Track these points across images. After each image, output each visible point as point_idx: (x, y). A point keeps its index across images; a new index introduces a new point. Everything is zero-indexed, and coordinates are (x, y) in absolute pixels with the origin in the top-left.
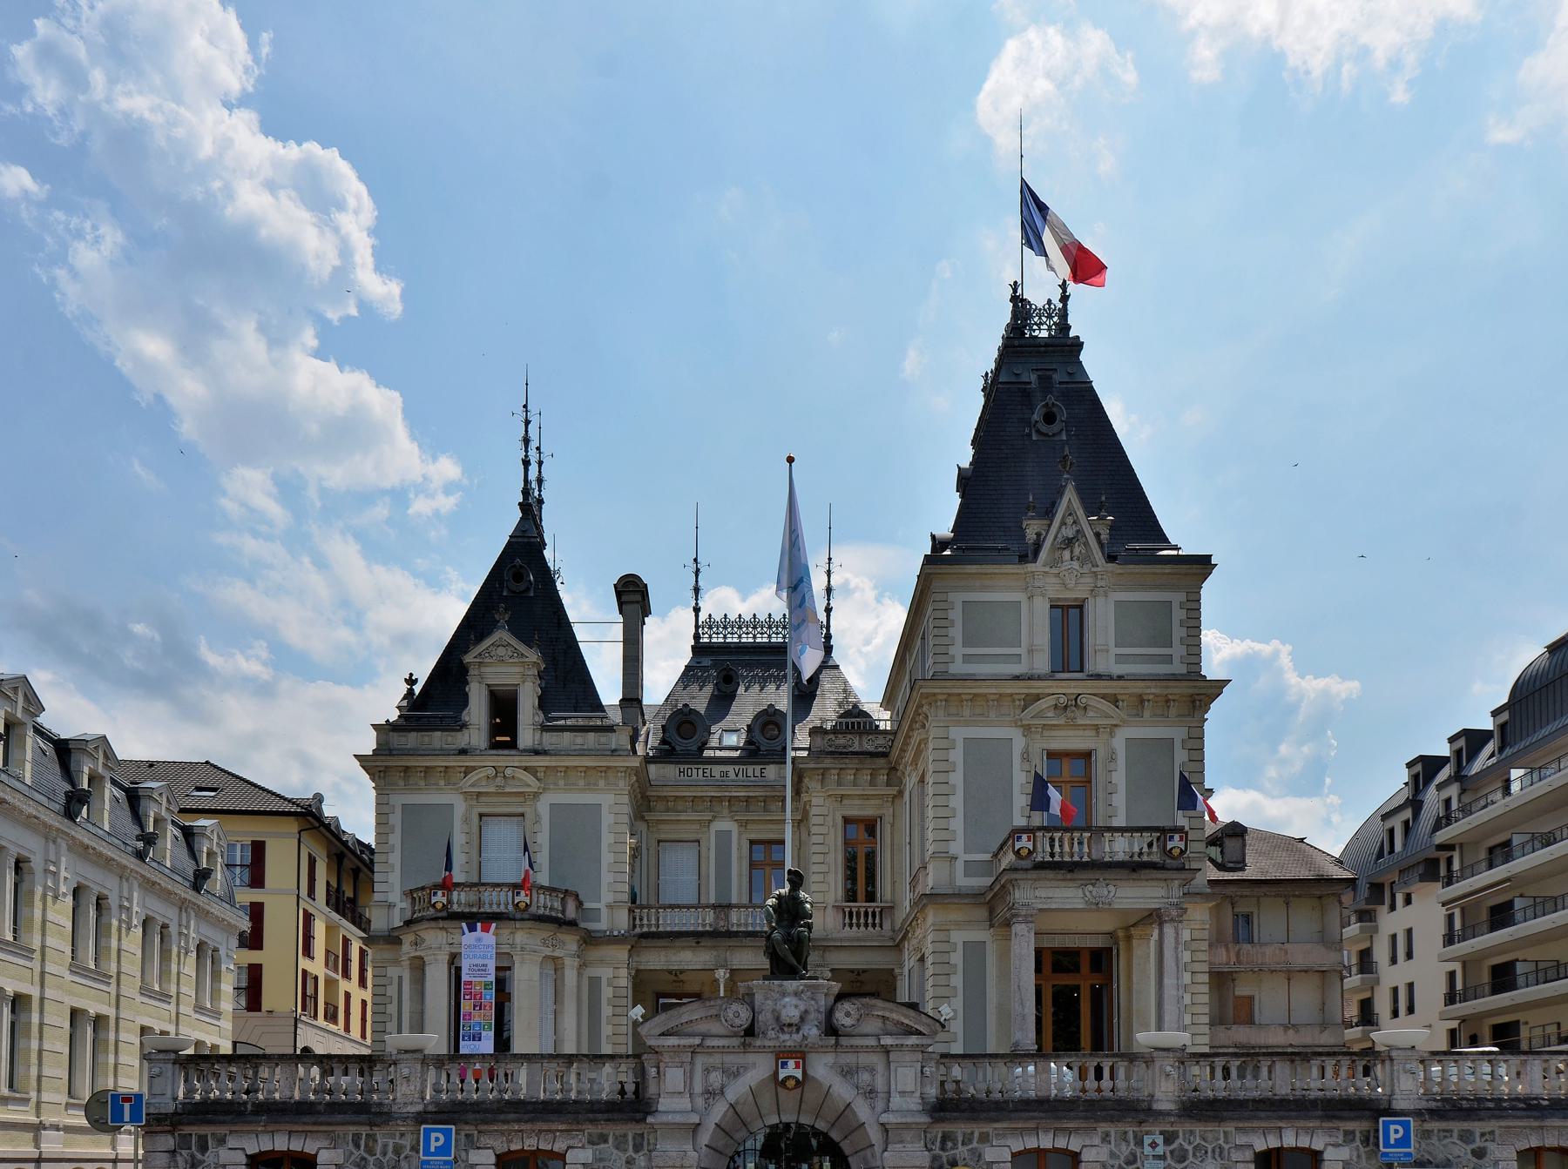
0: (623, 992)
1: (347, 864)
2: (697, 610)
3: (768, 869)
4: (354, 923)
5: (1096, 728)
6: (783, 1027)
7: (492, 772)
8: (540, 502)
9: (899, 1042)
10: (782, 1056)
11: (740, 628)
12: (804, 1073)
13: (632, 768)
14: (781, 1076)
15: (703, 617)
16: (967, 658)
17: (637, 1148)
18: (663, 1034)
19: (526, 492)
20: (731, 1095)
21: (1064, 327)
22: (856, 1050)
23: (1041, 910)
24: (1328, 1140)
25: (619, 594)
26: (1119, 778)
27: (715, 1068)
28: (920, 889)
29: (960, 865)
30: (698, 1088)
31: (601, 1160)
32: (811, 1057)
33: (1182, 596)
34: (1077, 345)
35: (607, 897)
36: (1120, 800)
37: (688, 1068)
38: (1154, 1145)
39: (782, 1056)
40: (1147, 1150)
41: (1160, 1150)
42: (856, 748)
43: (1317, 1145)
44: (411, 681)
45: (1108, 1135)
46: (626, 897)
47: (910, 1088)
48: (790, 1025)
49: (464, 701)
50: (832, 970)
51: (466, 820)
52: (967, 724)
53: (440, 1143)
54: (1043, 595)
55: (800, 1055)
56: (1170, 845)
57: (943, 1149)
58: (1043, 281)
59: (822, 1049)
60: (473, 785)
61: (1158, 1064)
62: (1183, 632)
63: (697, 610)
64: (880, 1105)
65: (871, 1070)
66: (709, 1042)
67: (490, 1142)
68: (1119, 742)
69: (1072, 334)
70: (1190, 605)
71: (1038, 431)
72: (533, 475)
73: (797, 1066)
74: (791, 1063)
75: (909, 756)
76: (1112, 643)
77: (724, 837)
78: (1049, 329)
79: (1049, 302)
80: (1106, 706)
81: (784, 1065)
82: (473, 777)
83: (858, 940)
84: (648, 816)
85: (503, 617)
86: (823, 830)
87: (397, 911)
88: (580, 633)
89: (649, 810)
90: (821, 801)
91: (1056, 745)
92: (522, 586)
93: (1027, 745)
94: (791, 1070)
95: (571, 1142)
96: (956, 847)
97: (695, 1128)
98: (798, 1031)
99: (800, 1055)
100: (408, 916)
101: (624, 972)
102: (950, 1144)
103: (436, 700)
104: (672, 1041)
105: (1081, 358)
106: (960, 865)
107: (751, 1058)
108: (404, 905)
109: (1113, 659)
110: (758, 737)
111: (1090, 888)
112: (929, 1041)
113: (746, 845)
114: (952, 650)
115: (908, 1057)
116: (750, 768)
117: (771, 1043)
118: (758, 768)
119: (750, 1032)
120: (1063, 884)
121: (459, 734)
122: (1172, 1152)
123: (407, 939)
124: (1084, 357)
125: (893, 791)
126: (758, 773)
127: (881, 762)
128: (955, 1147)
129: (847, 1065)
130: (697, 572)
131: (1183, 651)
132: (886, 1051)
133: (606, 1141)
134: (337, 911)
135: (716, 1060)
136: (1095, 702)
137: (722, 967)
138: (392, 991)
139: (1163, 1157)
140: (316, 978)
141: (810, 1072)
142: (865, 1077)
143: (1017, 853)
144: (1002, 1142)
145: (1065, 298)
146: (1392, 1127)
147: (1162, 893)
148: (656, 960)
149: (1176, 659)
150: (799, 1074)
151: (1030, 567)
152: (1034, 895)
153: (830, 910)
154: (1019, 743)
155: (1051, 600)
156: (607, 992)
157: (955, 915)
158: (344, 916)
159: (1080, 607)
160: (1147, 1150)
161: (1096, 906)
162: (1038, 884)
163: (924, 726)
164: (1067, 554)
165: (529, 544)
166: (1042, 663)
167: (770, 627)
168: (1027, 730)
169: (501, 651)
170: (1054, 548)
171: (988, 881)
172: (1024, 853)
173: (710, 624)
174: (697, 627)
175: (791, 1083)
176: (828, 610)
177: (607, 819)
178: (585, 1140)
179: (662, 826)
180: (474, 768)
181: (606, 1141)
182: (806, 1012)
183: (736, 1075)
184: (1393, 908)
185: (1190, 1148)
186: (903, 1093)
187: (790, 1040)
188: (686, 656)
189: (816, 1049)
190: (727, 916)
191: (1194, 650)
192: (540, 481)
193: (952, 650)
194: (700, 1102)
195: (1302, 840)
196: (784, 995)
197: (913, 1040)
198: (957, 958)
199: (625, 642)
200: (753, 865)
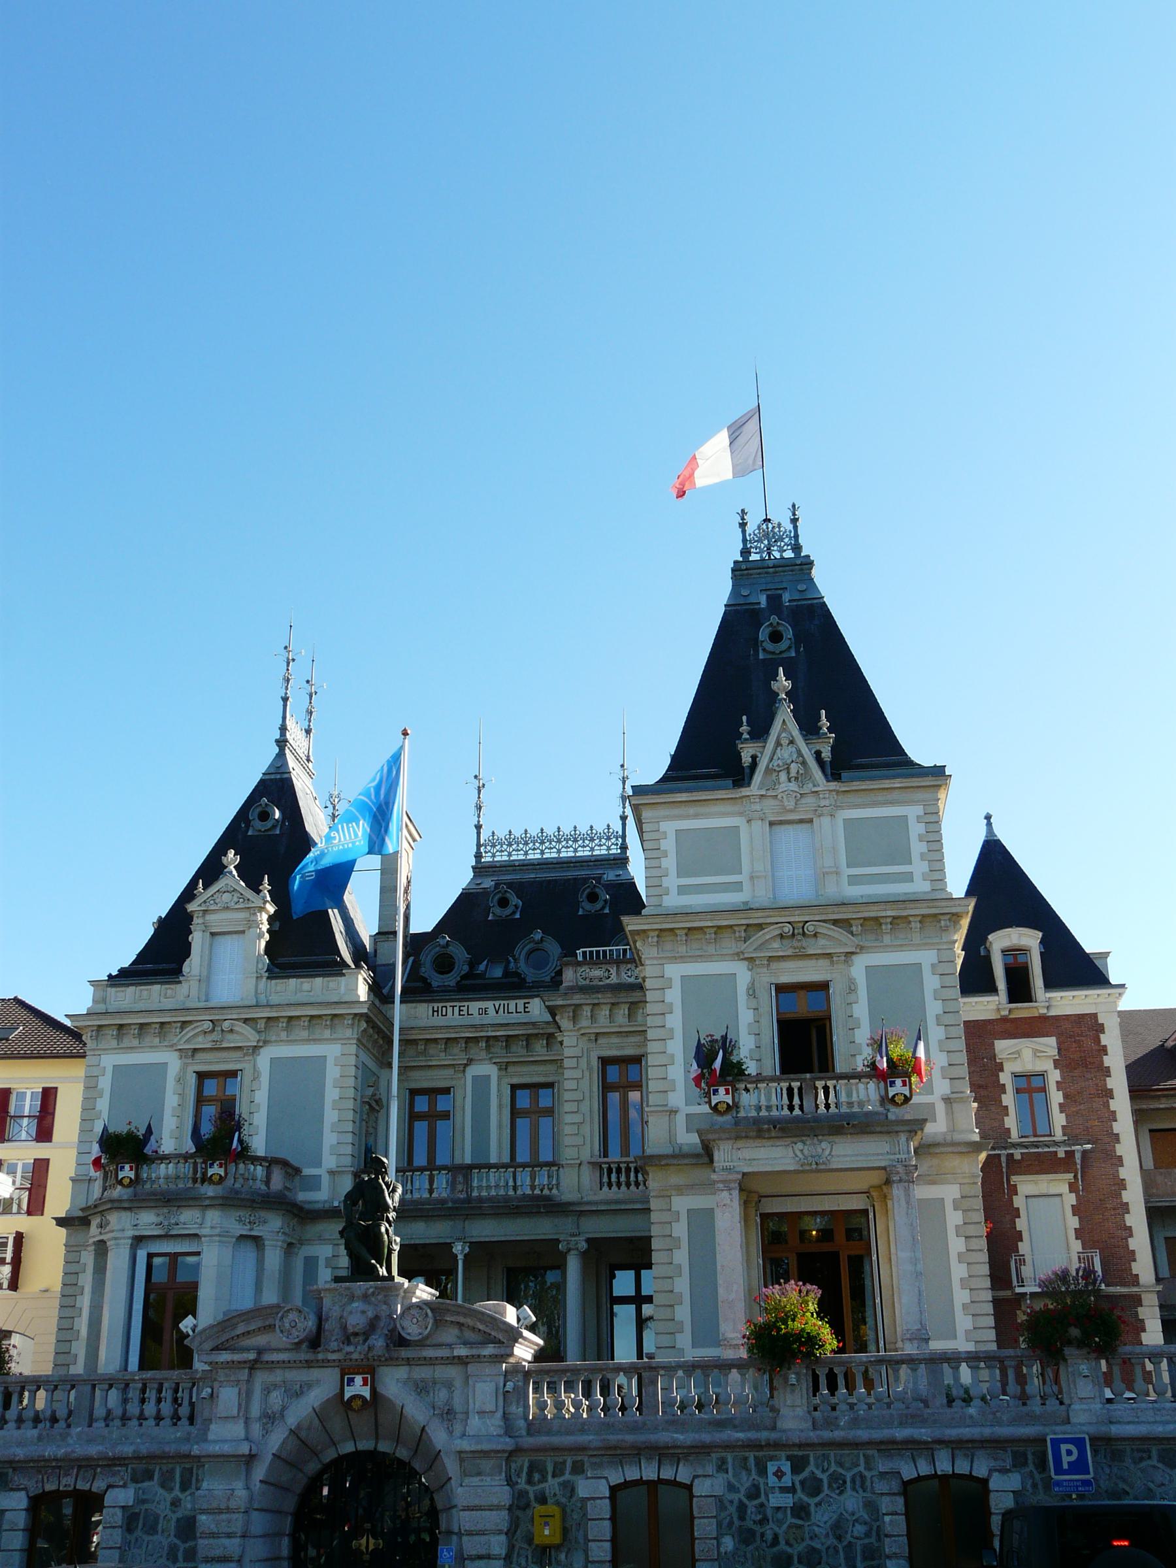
2: (478, 827)
5: (829, 956)
6: (348, 1338)
9: (475, 1352)
10: (347, 1372)
12: (374, 1391)
13: (361, 1015)
14: (347, 1396)
16: (682, 890)
17: (184, 1488)
20: (292, 1420)
21: (797, 548)
22: (431, 1362)
24: (992, 1464)
29: (680, 1120)
30: (255, 1411)
31: (144, 1501)
33: (918, 810)
35: (329, 1161)
37: (244, 1388)
38: (779, 1474)
39: (347, 1372)
40: (772, 1480)
41: (787, 1481)
42: (614, 979)
43: (980, 1471)
45: (723, 1461)
47: (490, 1407)
48: (356, 1334)
50: (588, 1240)
51: (179, 1080)
52: (682, 959)
53: (1073, 1458)
55: (369, 1370)
57: (529, 1482)
59: (391, 1361)
60: (187, 1041)
62: (922, 847)
63: (478, 827)
66: (268, 1357)
67: (25, 1482)
68: (859, 967)
73: (365, 1384)
74: (359, 1379)
77: (481, 1083)
82: (189, 1032)
83: (617, 1202)
86: (577, 1074)
91: (785, 979)
95: (111, 1480)
97: (251, 1458)
98: (365, 1341)
99: (369, 1370)
102: (537, 1476)
106: (680, 1120)
107: (315, 1374)
113: (507, 1092)
114: (666, 882)
116: (512, 1003)
118: (521, 1003)
119: (315, 1341)
120: (758, 1142)
122: (802, 1483)
123: (95, 1222)
124: (815, 572)
126: (521, 1009)
128: (544, 1479)
131: (924, 867)
132: (462, 1361)
133: (151, 1478)
135: (278, 1376)
136: (823, 929)
137: (459, 1239)
139: (792, 1490)
141: (381, 1389)
144: (599, 1473)
146: (1064, 1447)
147: (886, 1147)
149: (917, 877)
150: (366, 1392)
151: (745, 791)
160: (772, 1480)
162: (740, 1144)
164: (783, 776)
165: (282, 780)
169: (226, 897)
170: (768, 771)
174: (479, 845)
175: (357, 1404)
176: (624, 818)
178: (127, 1477)
181: (151, 1478)
182: (377, 1318)
183: (299, 1394)
185: (824, 1477)
186: (481, 1413)
187: (356, 1352)
191: (937, 866)
193: (666, 882)
194: (256, 1428)
196: (352, 1298)
200: (515, 1113)
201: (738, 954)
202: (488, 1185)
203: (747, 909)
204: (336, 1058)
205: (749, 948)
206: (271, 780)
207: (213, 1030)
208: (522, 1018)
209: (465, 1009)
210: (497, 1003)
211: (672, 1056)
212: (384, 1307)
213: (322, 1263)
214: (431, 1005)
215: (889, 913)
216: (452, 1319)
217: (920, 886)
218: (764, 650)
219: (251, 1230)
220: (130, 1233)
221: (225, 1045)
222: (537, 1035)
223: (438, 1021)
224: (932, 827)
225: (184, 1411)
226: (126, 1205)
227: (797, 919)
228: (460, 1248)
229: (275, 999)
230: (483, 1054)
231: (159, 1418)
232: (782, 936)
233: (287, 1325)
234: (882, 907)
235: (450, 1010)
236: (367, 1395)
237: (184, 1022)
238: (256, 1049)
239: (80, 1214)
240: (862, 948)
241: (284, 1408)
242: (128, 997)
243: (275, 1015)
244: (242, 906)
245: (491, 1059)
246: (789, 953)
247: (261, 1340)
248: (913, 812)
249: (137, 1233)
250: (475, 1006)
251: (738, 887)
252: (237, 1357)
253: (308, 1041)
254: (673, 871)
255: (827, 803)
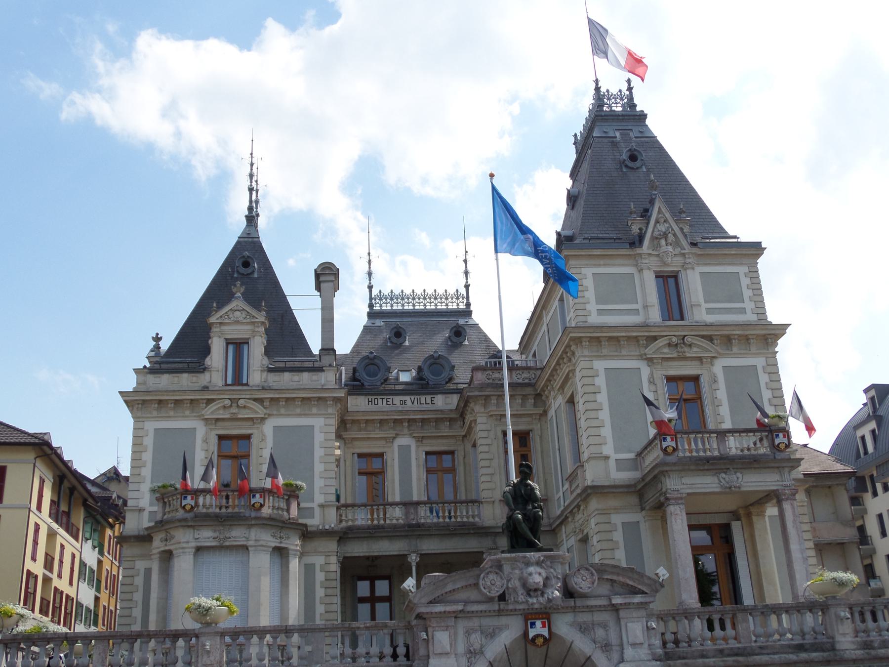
0: (333, 576)
1: (66, 484)
2: (370, 287)
3: (440, 473)
4: (67, 530)
5: (700, 359)
6: (530, 591)
7: (228, 402)
8: (258, 215)
9: (627, 601)
10: (530, 617)
11: (403, 299)
15: (375, 292)
16: (600, 312)
18: (431, 602)
19: (250, 209)
22: (591, 609)
23: (688, 494)
25: (317, 276)
26: (722, 394)
27: (475, 631)
28: (580, 484)
29: (612, 463)
32: (555, 617)
34: (643, 116)
36: (725, 410)
37: (452, 631)
39: (530, 617)
44: (157, 339)
46: (334, 498)
48: (536, 590)
49: (207, 351)
51: (205, 441)
54: (649, 269)
56: (777, 441)
58: (614, 81)
61: (832, 611)
63: (370, 287)
64: (616, 656)
65: (605, 626)
66: (470, 608)
68: (718, 367)
69: (638, 109)
70: (752, 275)
71: (626, 166)
72: (254, 198)
73: (544, 626)
74: (539, 623)
75: (558, 383)
76: (702, 301)
78: (623, 106)
79: (620, 91)
80: (705, 343)
81: (533, 625)
82: (213, 407)
84: (346, 435)
85: (239, 291)
86: (488, 441)
87: (146, 515)
88: (293, 302)
89: (346, 430)
90: (484, 420)
91: (672, 373)
92: (249, 270)
93: (652, 374)
94: (539, 629)
96: (608, 450)
100: (159, 517)
101: (334, 559)
103: (189, 347)
104: (439, 608)
105: (647, 123)
107: (504, 620)
108: (155, 508)
109: (704, 311)
110: (427, 374)
111: (723, 475)
112: (651, 599)
114: (588, 307)
115: (635, 614)
117: (521, 607)
118: (429, 398)
121: (201, 376)
124: (648, 122)
125: (540, 411)
126: (429, 401)
127: (529, 390)
129: (584, 623)
130: (370, 262)
132: (615, 609)
134: (57, 522)
135: (475, 623)
137: (414, 552)
138: (139, 581)
140: (36, 577)
141: (553, 629)
142: (600, 633)
143: (665, 450)
145: (630, 89)
148: (359, 549)
149: (748, 311)
150: (545, 632)
151: (638, 251)
152: (674, 484)
153: (497, 504)
154: (645, 371)
155: (655, 272)
156: (320, 576)
157: (612, 502)
158: (61, 526)
159: (675, 276)
161: (729, 490)
163: (570, 360)
164: (663, 242)
165: (253, 242)
166: (655, 315)
167: (425, 299)
168: (650, 361)
169: (238, 314)
170: (653, 238)
171: (637, 475)
172: (670, 450)
173: (381, 297)
174: (371, 299)
175: (540, 641)
177: (319, 438)
179: (356, 443)
180: (213, 400)
184: (875, 494)
186: (634, 645)
188: (364, 320)
189: (558, 610)
190: (417, 512)
192: (257, 202)
195: (805, 446)
196: (528, 564)
197: (638, 599)
198: (618, 536)
199: (323, 309)
200: (429, 471)
201: (641, 356)
202: (424, 515)
203: (645, 326)
204: (320, 427)
205: (650, 351)
206: (245, 242)
207: (231, 406)
208: (431, 407)
209: (390, 400)
210: (413, 398)
211: (603, 421)
212: (552, 570)
213: (318, 568)
214: (367, 398)
215: (738, 332)
216: (609, 577)
217: (750, 317)
218: (238, 271)
219: (281, 543)
220: (193, 544)
221: (240, 416)
222: (442, 419)
223: (372, 407)
224: (755, 281)
225: (401, 650)
226: (190, 524)
227: (680, 333)
228: (414, 558)
229: (275, 385)
230: (406, 431)
231: (381, 657)
232: (669, 345)
233: (489, 583)
234: (734, 327)
235: (380, 401)
236: (546, 634)
237: (208, 400)
238: (263, 419)
239: (146, 533)
240: (269, 415)
241: (482, 646)
242: (164, 381)
243: (277, 396)
244: (248, 320)
245: (411, 434)
246: (675, 355)
247: (463, 595)
248: (742, 270)
249: (199, 544)
250: (397, 399)
251: (636, 312)
252: (449, 608)
253: (300, 415)
254: (593, 299)
255: (690, 261)
